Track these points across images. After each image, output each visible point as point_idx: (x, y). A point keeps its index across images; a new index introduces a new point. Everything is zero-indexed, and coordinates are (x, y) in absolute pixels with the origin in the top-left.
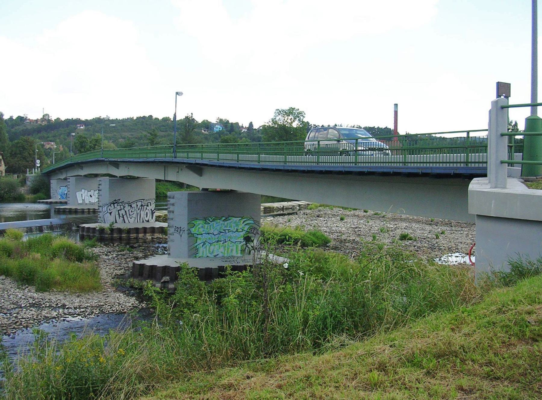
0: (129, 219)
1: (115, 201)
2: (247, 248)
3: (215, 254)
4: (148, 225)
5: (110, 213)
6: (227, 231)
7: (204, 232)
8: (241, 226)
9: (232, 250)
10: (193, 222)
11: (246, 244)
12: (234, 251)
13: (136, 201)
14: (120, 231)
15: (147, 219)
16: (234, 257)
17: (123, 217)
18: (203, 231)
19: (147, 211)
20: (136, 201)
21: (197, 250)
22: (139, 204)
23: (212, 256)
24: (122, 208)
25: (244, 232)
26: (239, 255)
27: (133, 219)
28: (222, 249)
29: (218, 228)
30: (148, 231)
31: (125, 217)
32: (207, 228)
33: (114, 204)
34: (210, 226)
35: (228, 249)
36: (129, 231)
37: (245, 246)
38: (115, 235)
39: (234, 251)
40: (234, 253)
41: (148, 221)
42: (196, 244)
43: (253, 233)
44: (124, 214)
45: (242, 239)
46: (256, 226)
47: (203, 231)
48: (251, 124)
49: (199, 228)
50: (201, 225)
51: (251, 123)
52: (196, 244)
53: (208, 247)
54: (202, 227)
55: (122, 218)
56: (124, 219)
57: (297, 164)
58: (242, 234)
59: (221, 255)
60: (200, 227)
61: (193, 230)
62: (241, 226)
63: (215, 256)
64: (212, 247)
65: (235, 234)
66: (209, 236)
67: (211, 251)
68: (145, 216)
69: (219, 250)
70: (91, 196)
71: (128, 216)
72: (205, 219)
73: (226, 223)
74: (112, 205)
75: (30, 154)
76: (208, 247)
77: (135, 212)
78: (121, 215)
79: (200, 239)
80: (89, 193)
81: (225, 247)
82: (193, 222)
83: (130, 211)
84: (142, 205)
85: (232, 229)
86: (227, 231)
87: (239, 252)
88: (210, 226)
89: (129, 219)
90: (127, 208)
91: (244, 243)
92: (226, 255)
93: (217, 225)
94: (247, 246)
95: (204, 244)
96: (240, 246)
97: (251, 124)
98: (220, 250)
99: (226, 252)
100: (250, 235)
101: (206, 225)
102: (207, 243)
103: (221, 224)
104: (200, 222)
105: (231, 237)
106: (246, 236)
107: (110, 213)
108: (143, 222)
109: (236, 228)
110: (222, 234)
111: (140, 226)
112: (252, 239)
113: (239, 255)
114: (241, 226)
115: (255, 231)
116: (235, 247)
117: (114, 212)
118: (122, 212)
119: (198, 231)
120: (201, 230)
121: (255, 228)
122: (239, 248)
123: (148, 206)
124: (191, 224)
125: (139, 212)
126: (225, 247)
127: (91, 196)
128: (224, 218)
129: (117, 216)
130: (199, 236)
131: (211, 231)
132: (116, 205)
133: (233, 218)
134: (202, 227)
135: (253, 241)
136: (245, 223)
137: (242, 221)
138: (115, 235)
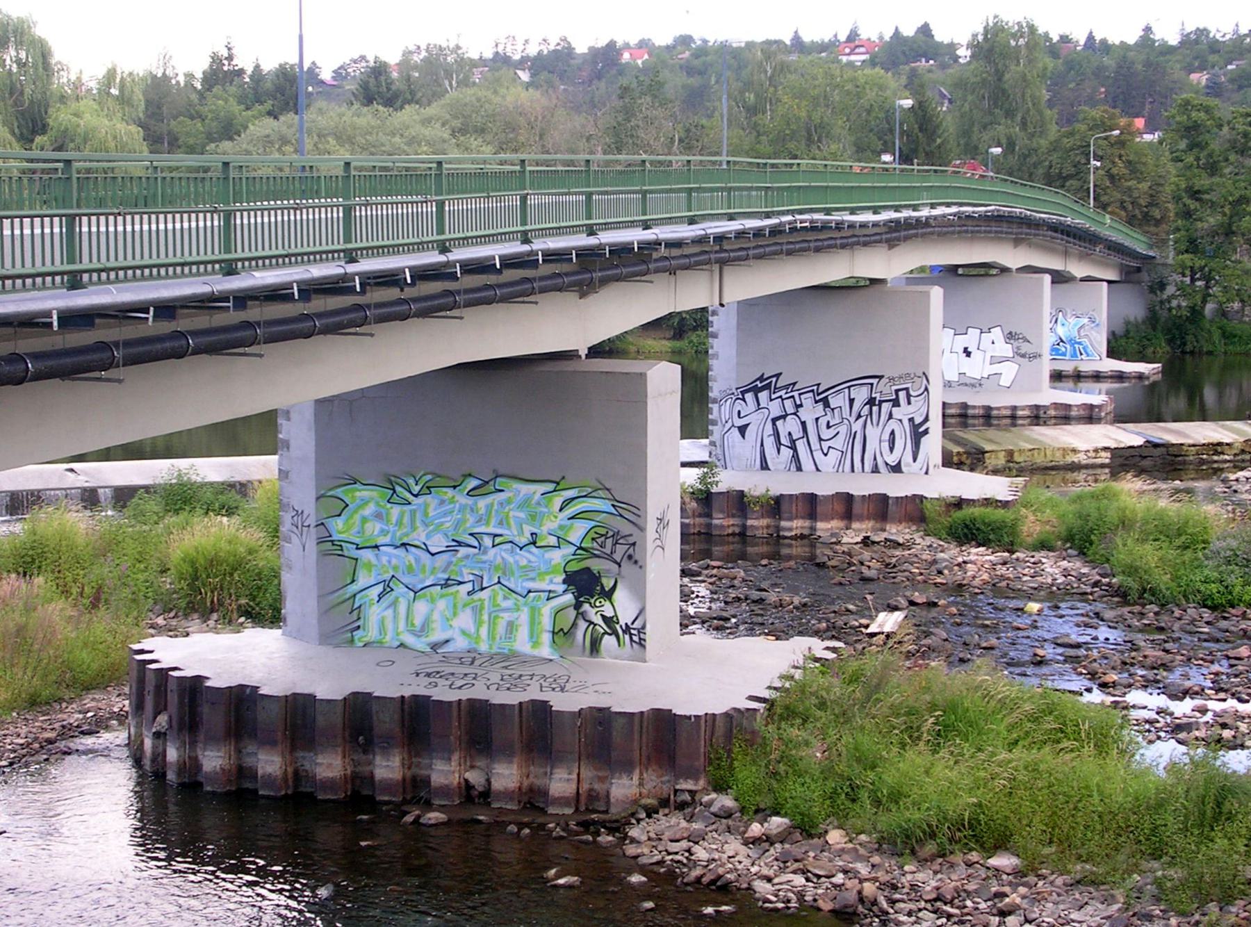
0: (818, 455)
1: (761, 379)
2: (582, 625)
3: (436, 636)
4: (895, 487)
5: (742, 430)
6: (488, 541)
7: (387, 540)
8: (552, 523)
9: (511, 627)
10: (339, 492)
11: (578, 606)
12: (523, 633)
13: (850, 383)
14: (739, 502)
15: (892, 459)
16: (524, 660)
17: (793, 447)
18: (383, 532)
19: (893, 425)
20: (850, 383)
21: (357, 612)
22: (861, 395)
23: (421, 644)
24: (790, 409)
26: (546, 651)
28: (465, 620)
29: (448, 524)
30: (857, 508)
31: (801, 446)
32: (399, 523)
33: (756, 391)
34: (413, 513)
36: (776, 506)
37: (573, 613)
38: (719, 520)
39: (523, 633)
40: (521, 643)
41: (897, 469)
42: (354, 588)
43: (609, 557)
45: (557, 583)
46: (626, 528)
47: (383, 532)
48: (257, 66)
49: (364, 520)
50: (369, 510)
52: (354, 588)
53: (402, 608)
54: (378, 516)
55: (787, 453)
56: (796, 457)
57: (1124, 229)
58: (557, 557)
59: (460, 644)
60: (367, 515)
61: (338, 526)
62: (550, 524)
63: (435, 647)
64: (421, 608)
65: (524, 558)
66: (409, 557)
67: (418, 622)
68: (886, 445)
69: (454, 623)
70: (967, 353)
72: (391, 484)
73: (482, 503)
74: (749, 397)
75: (1112, 177)
76: (402, 608)
77: (843, 429)
79: (369, 566)
80: (961, 342)
82: (339, 492)
83: (823, 422)
84: (871, 402)
85: (509, 533)
86: (488, 541)
87: (546, 638)
88: (413, 513)
89: (818, 455)
90: (810, 411)
91: (569, 598)
92: (483, 647)
93: (442, 515)
94: (583, 615)
95: (387, 589)
96: (547, 610)
97: (257, 66)
98: (455, 623)
99: (484, 631)
100: (596, 565)
101: (395, 511)
102: (399, 589)
103: (462, 509)
104: (365, 493)
105: (506, 569)
107: (742, 430)
108: (875, 470)
109: (528, 529)
110: (463, 551)
111: (863, 486)
112: (608, 583)
113: (546, 651)
114: (552, 523)
115: (620, 550)
116: (524, 616)
117: (756, 421)
118: (790, 426)
119: (361, 532)
120: (373, 528)
121: (617, 537)
122: (546, 622)
123: (896, 403)
124: (331, 501)
126: (477, 611)
127: (967, 353)
128: (473, 483)
129: (769, 443)
130: (367, 555)
131: (419, 536)
132: (763, 396)
133: (516, 485)
135: (609, 595)
136: (570, 511)
137: (558, 500)
138: (719, 520)
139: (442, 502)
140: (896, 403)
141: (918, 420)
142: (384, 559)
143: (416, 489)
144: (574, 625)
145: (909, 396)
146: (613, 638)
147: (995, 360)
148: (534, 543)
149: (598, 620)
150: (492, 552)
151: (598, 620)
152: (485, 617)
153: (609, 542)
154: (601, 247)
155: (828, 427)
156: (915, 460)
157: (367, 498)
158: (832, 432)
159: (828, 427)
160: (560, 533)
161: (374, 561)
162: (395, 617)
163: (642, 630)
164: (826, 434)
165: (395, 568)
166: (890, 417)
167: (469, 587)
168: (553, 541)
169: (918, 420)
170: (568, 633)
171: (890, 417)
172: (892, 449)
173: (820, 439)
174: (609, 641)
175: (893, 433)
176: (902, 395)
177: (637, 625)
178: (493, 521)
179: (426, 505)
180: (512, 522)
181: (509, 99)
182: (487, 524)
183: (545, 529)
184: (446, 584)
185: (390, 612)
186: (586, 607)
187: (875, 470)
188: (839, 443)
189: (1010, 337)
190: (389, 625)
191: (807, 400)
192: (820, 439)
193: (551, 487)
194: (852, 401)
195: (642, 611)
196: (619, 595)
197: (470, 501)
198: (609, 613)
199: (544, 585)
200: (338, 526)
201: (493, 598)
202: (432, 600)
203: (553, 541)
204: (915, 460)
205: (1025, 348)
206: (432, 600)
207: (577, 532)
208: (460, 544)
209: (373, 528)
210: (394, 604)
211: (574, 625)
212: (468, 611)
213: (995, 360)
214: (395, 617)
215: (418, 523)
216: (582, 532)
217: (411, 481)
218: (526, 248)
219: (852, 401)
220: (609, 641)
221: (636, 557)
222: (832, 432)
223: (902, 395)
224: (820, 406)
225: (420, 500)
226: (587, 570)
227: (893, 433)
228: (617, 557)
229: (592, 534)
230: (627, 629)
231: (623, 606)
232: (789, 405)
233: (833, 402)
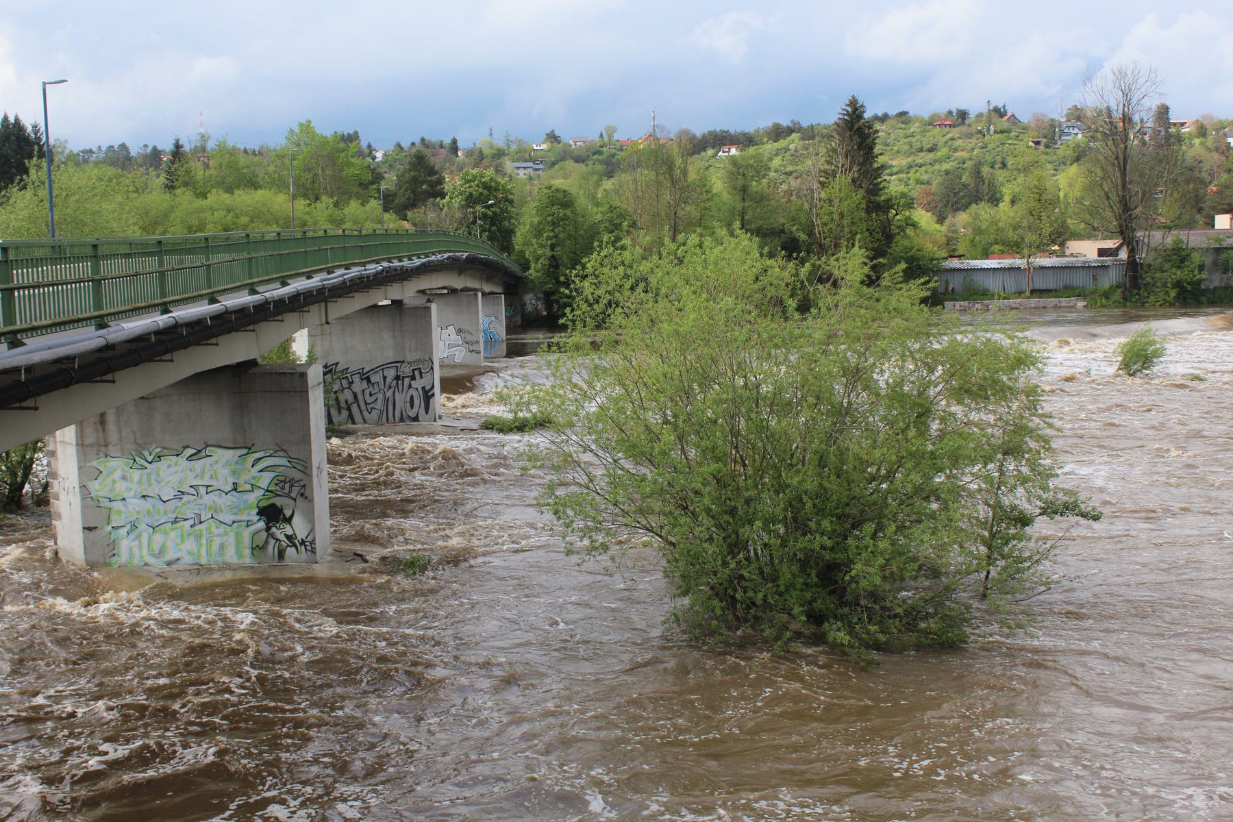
2: (272, 542)
3: (170, 556)
11: (268, 529)
13: (383, 367)
17: (349, 409)
19: (412, 392)
22: (391, 374)
25: (258, 493)
27: (375, 413)
28: (189, 545)
31: (354, 408)
32: (140, 482)
34: (149, 475)
35: (209, 545)
37: (265, 534)
43: (288, 496)
44: (351, 399)
50: (117, 475)
51: (177, 141)
53: (145, 540)
54: (124, 478)
55: (345, 413)
58: (254, 497)
59: (188, 560)
64: (158, 539)
67: (156, 548)
71: (363, 407)
73: (198, 465)
76: (145, 540)
77: (380, 396)
78: (343, 404)
79: (119, 513)
81: (198, 537)
83: (367, 392)
84: (397, 378)
86: (203, 490)
87: (247, 552)
88: (149, 475)
89: (366, 413)
91: (262, 524)
92: (203, 561)
96: (246, 534)
100: (279, 502)
106: (263, 504)
109: (231, 480)
110: (186, 498)
112: (288, 513)
116: (232, 539)
121: (292, 482)
122: (246, 540)
123: (413, 378)
125: (389, 394)
126: (198, 537)
133: (220, 451)
134: (124, 478)
135: (288, 521)
139: (169, 466)
140: (413, 378)
141: (428, 388)
142: (130, 508)
143: (150, 459)
144: (267, 542)
145: (421, 373)
146: (293, 549)
147: (450, 346)
148: (235, 489)
149: (282, 537)
150: (206, 497)
151: (282, 537)
152: (204, 541)
153: (287, 485)
154: (267, 302)
155: (371, 395)
156: (427, 412)
157: (116, 467)
158: (373, 398)
159: (371, 395)
160: (253, 482)
161: (123, 509)
162: (140, 547)
163: (313, 542)
164: (369, 400)
165: (138, 513)
166: (410, 386)
167: (191, 522)
168: (249, 487)
169: (428, 388)
170: (262, 548)
171: (410, 386)
172: (412, 407)
173: (366, 404)
174: (291, 551)
175: (412, 397)
176: (417, 373)
177: (310, 539)
178: (207, 476)
179: (159, 469)
180: (219, 477)
181: (1022, 380)
182: (202, 478)
183: (242, 480)
184: (175, 521)
185: (136, 543)
186: (274, 529)
187: (402, 420)
188: (379, 405)
189: (459, 331)
190: (136, 551)
191: (356, 379)
192: (366, 404)
193: (245, 451)
194: (385, 378)
195: (312, 530)
196: (295, 520)
197: (190, 464)
198: (290, 532)
199: (244, 517)
200: (95, 487)
201: (208, 529)
202: (166, 533)
203: (249, 487)
204: (427, 412)
205: (469, 338)
206: (166, 533)
207: (265, 480)
208: (183, 493)
209: (121, 487)
210: (139, 537)
211: (267, 542)
212: (192, 538)
213: (450, 346)
214: (140, 547)
215: (153, 482)
216: (268, 481)
217: (146, 453)
218: (216, 307)
219: (385, 378)
220: (291, 551)
221: (307, 494)
222: (373, 398)
223: (417, 373)
224: (365, 383)
225: (154, 465)
226: (273, 505)
227: (412, 397)
228: (293, 495)
229: (275, 481)
230: (303, 542)
231: (299, 527)
232: (344, 382)
233: (373, 379)
